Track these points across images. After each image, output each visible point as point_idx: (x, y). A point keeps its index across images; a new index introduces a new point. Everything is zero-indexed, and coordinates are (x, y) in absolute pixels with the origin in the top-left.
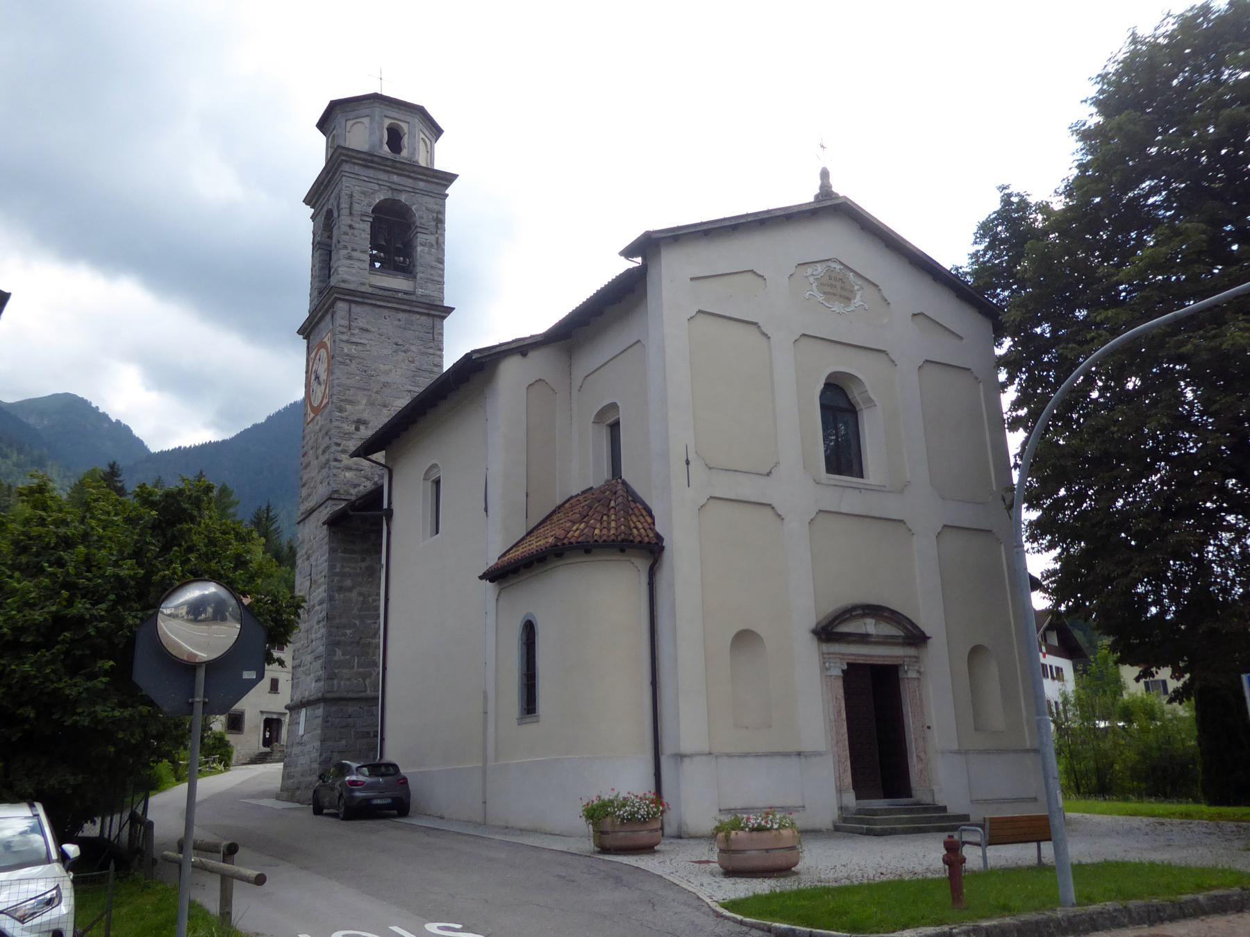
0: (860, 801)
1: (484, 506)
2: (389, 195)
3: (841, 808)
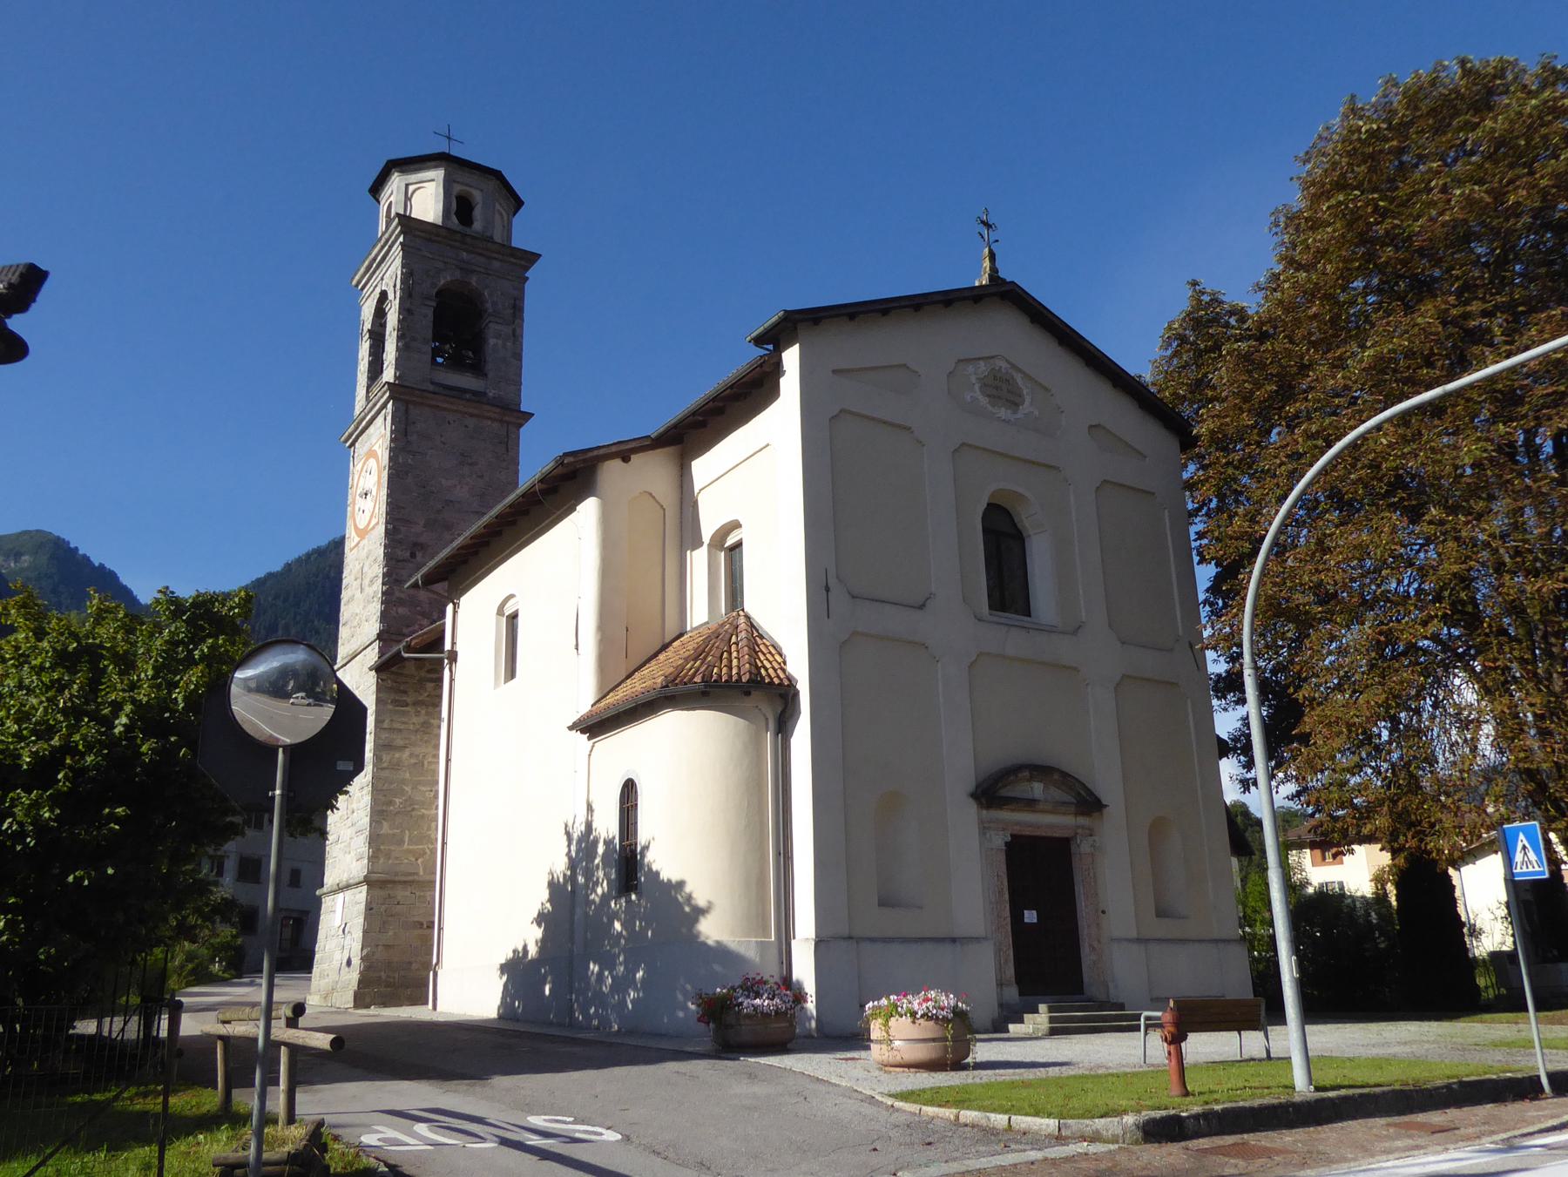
0: (1025, 998)
1: (575, 643)
2: (458, 275)
3: (1001, 1005)
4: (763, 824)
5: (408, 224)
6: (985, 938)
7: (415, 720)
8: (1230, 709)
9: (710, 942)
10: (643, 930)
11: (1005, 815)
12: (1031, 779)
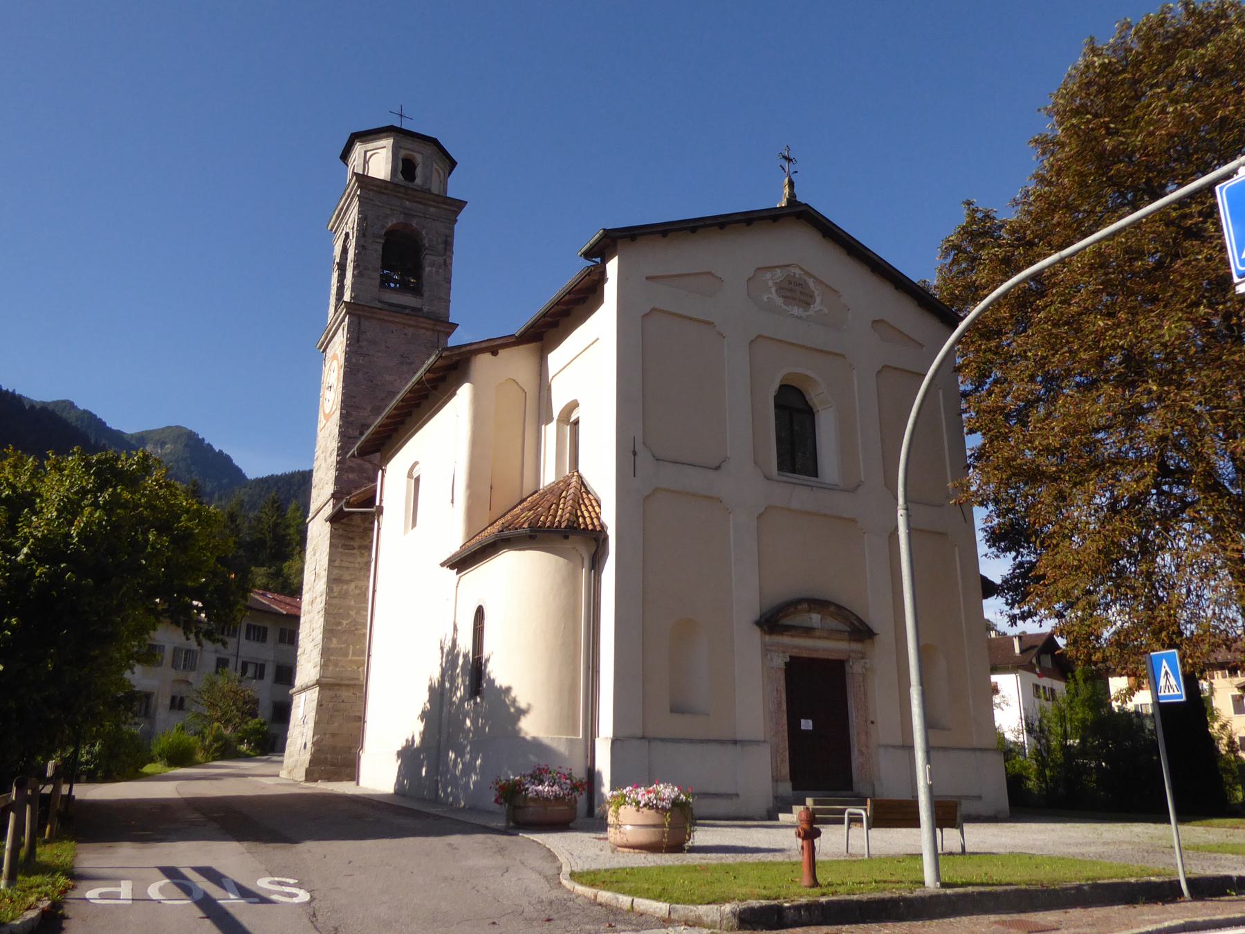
0: (798, 792)
2: (402, 219)
3: (776, 798)
4: (576, 643)
5: (364, 180)
6: (765, 741)
7: (359, 560)
8: (1002, 556)
9: (528, 737)
10: (484, 726)
11: (786, 640)
12: (809, 611)
